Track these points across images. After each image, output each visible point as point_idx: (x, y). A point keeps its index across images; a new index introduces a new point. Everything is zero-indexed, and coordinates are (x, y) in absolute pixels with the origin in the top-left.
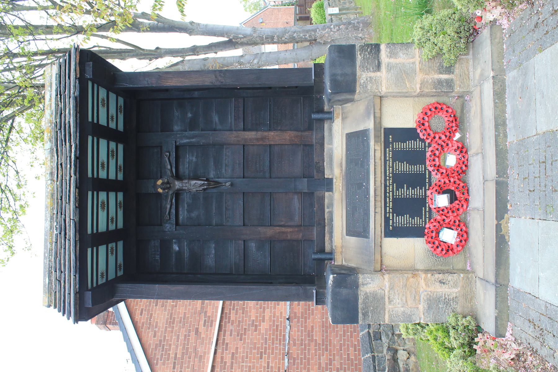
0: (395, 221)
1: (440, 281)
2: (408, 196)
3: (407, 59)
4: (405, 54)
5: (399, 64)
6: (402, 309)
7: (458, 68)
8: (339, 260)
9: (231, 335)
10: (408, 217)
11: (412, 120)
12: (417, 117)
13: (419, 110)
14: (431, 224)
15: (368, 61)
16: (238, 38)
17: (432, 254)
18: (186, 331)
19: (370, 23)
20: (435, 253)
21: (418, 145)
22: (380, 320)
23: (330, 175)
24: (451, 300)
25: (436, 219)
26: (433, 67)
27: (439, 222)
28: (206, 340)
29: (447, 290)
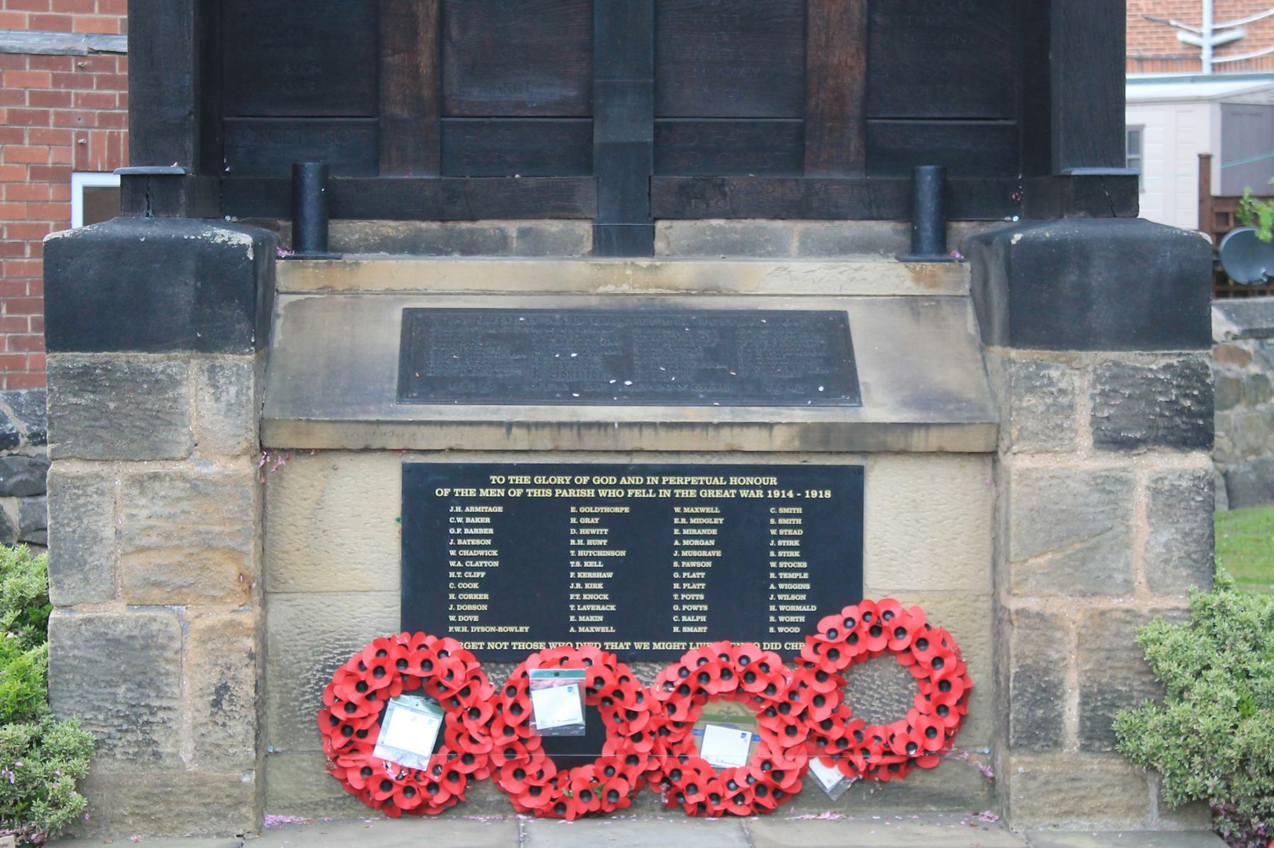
0: (472, 509)
1: (225, 688)
2: (578, 564)
3: (1145, 559)
4: (1169, 550)
5: (1123, 529)
6: (109, 532)
7: (1107, 772)
10: (487, 563)
11: (898, 587)
12: (907, 607)
13: (940, 616)
14: (457, 659)
15: (1141, 397)
17: (331, 667)
20: (337, 677)
21: (792, 608)
22: (62, 441)
23: (669, 243)
24: (144, 732)
25: (477, 678)
26: (1110, 668)
27: (466, 691)
29: (188, 717)
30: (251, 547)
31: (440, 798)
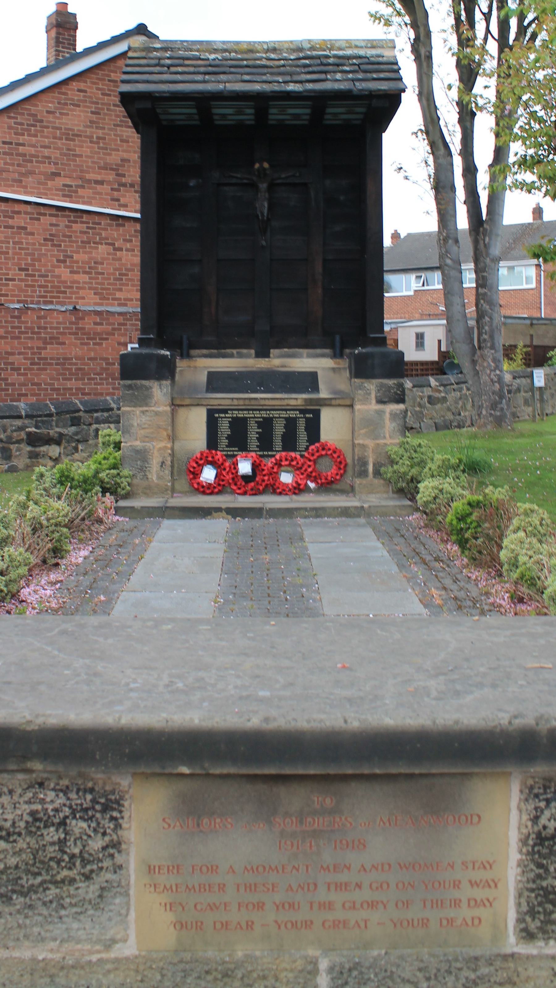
6: (136, 424)
8: (181, 364)
9: (51, 225)
13: (339, 446)
16: (484, 235)
18: (56, 158)
19: (500, 425)
20: (191, 460)
27: (222, 464)
28: (44, 189)
29: (155, 469)
30: (170, 428)
31: (216, 490)
